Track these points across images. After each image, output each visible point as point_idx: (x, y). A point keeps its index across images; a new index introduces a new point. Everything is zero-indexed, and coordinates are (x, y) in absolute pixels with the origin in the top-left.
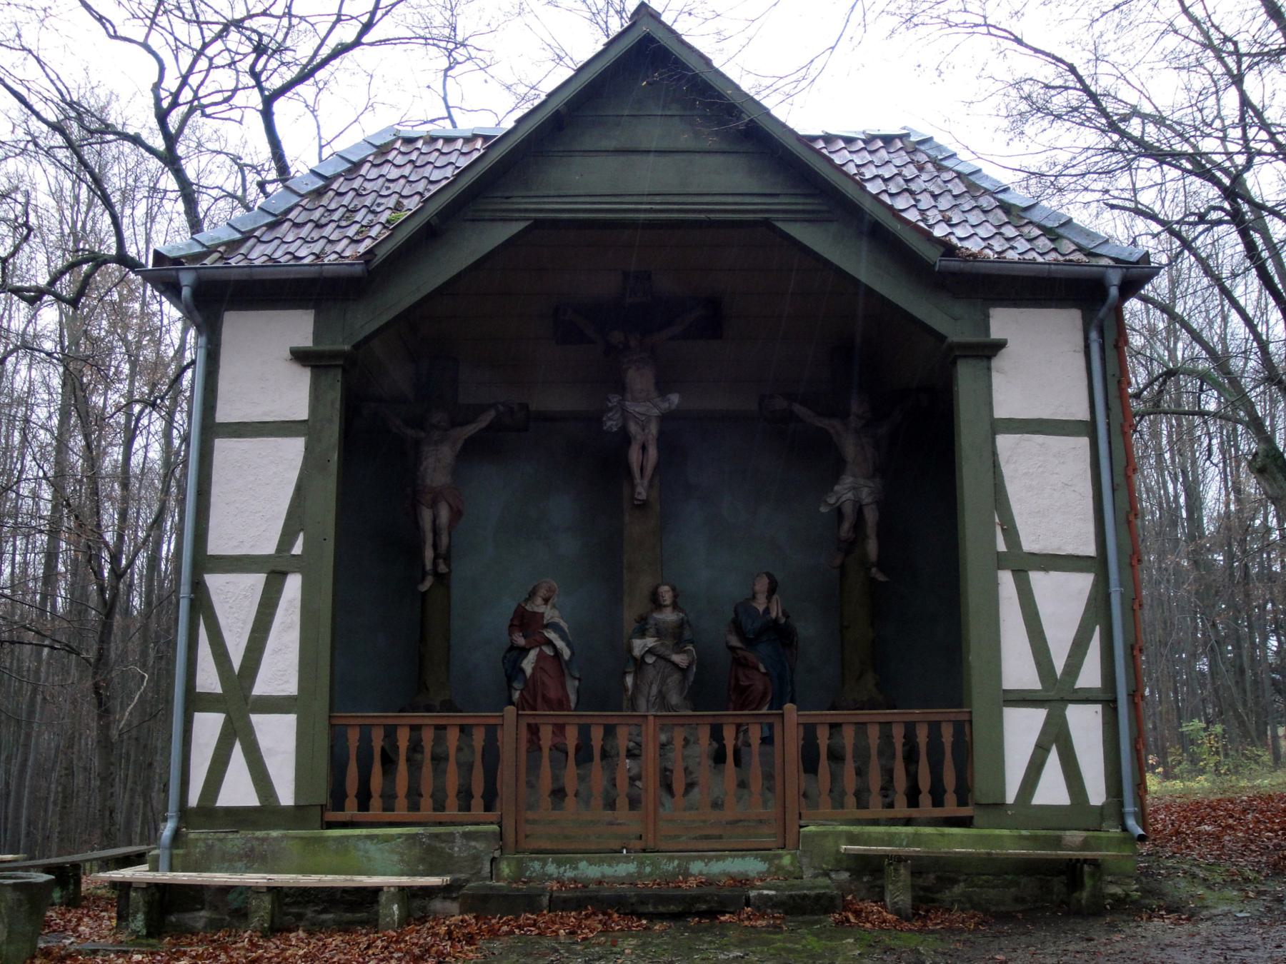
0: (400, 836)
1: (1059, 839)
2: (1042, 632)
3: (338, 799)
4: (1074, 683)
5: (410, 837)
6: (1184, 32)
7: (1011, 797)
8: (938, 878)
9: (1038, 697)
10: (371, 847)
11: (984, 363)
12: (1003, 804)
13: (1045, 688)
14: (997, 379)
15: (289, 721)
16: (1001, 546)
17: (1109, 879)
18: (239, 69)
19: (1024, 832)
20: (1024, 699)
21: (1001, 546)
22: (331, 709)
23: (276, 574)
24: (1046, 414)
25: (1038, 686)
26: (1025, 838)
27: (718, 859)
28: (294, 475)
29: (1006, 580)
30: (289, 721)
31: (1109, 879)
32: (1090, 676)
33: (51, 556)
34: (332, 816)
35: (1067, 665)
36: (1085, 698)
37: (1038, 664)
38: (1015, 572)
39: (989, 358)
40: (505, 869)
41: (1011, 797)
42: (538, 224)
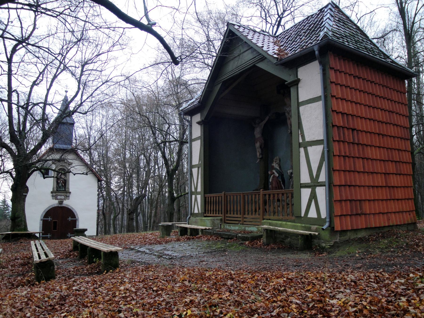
0: (209, 219)
1: (310, 228)
2: (311, 165)
3: (205, 210)
4: (318, 180)
5: (211, 219)
6: (27, 32)
7: (303, 215)
8: (285, 236)
9: (309, 185)
10: (207, 221)
11: (296, 86)
12: (301, 217)
13: (311, 183)
14: (300, 90)
15: (302, 181)
16: (301, 141)
17: (322, 241)
18: (126, 81)
19: (303, 225)
20: (306, 186)
21: (301, 141)
22: (204, 194)
23: (199, 168)
24: (311, 97)
25: (310, 182)
26: (303, 227)
27: (249, 227)
28: (199, 147)
29: (302, 150)
30: (302, 181)
31: (322, 241)
32: (323, 178)
33: (416, 129)
34: (207, 214)
35: (316, 175)
36: (321, 185)
37: (310, 175)
38: (304, 148)
39: (297, 84)
40: (222, 227)
41: (303, 215)
42: (223, 82)
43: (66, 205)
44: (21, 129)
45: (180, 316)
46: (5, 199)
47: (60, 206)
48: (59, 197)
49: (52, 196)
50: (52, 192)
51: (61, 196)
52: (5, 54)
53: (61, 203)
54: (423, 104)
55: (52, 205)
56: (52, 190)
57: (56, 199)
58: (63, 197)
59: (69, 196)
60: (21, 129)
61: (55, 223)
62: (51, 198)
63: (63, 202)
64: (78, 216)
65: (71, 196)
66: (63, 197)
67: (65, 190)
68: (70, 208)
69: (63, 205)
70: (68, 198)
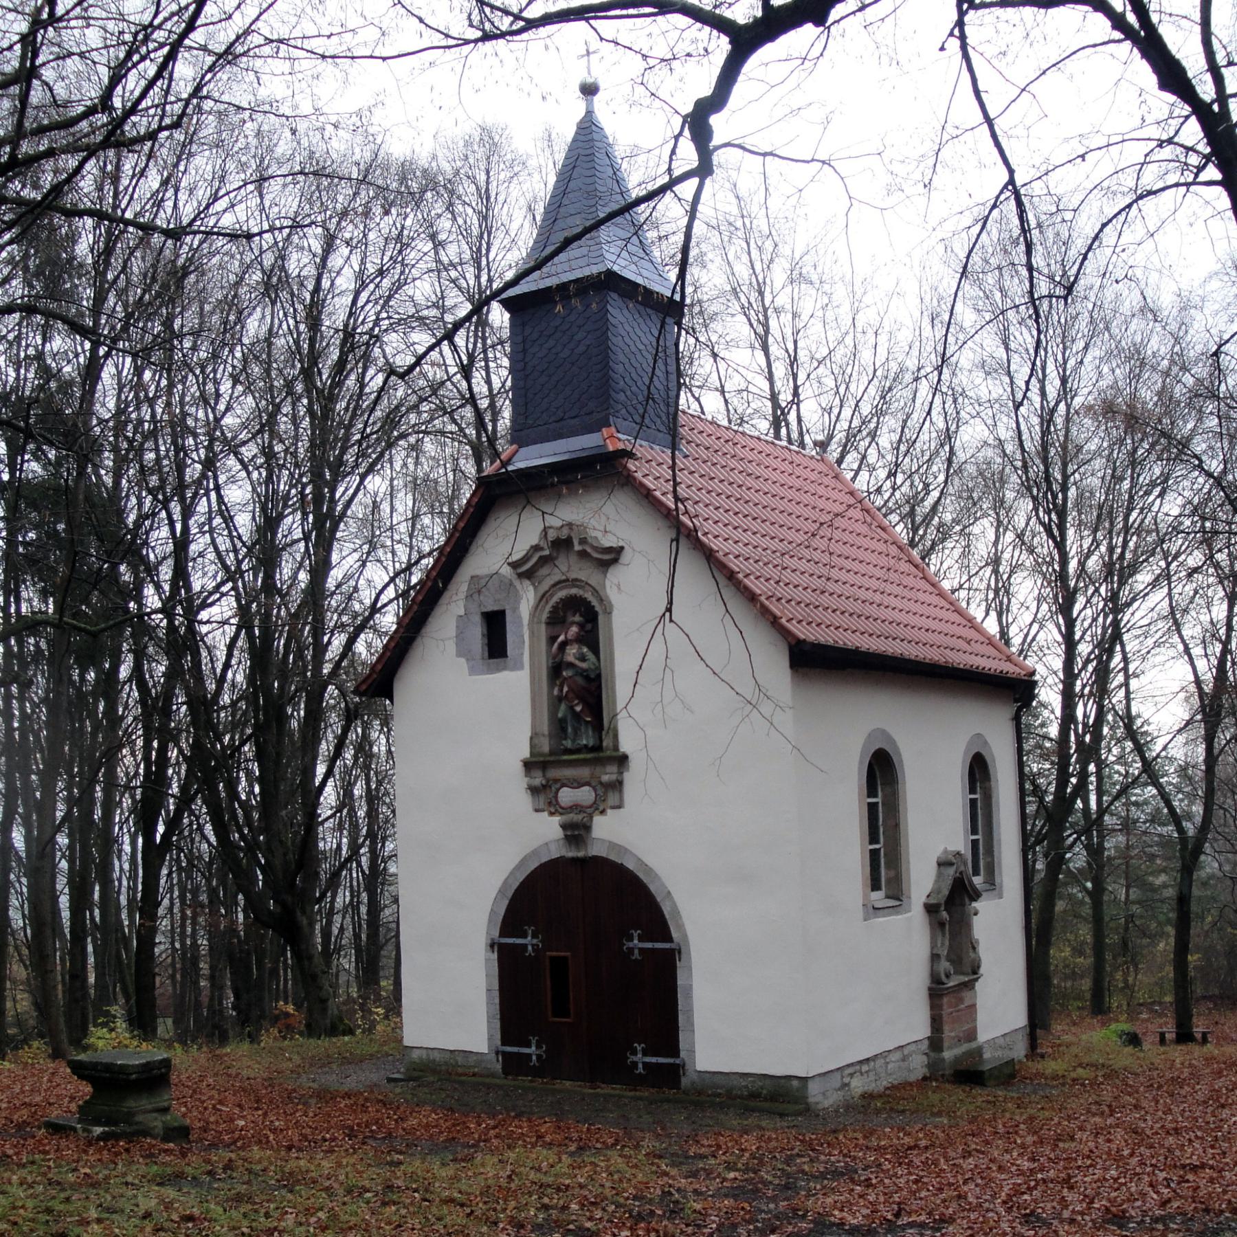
43: (613, 846)
44: (97, 919)
45: (1233, 925)
46: (588, 130)
47: (571, 854)
48: (567, 796)
49: (534, 790)
50: (528, 765)
51: (577, 784)
52: (747, 154)
53: (576, 832)
54: (4, 796)
55: (535, 853)
56: (526, 753)
57: (553, 807)
58: (585, 795)
59: (618, 785)
60: (97, 919)
61: (559, 966)
62: (524, 801)
63: (587, 828)
64: (681, 927)
65: (633, 779)
66: (585, 795)
67: (598, 748)
68: (630, 865)
69: (595, 850)
70: (612, 799)
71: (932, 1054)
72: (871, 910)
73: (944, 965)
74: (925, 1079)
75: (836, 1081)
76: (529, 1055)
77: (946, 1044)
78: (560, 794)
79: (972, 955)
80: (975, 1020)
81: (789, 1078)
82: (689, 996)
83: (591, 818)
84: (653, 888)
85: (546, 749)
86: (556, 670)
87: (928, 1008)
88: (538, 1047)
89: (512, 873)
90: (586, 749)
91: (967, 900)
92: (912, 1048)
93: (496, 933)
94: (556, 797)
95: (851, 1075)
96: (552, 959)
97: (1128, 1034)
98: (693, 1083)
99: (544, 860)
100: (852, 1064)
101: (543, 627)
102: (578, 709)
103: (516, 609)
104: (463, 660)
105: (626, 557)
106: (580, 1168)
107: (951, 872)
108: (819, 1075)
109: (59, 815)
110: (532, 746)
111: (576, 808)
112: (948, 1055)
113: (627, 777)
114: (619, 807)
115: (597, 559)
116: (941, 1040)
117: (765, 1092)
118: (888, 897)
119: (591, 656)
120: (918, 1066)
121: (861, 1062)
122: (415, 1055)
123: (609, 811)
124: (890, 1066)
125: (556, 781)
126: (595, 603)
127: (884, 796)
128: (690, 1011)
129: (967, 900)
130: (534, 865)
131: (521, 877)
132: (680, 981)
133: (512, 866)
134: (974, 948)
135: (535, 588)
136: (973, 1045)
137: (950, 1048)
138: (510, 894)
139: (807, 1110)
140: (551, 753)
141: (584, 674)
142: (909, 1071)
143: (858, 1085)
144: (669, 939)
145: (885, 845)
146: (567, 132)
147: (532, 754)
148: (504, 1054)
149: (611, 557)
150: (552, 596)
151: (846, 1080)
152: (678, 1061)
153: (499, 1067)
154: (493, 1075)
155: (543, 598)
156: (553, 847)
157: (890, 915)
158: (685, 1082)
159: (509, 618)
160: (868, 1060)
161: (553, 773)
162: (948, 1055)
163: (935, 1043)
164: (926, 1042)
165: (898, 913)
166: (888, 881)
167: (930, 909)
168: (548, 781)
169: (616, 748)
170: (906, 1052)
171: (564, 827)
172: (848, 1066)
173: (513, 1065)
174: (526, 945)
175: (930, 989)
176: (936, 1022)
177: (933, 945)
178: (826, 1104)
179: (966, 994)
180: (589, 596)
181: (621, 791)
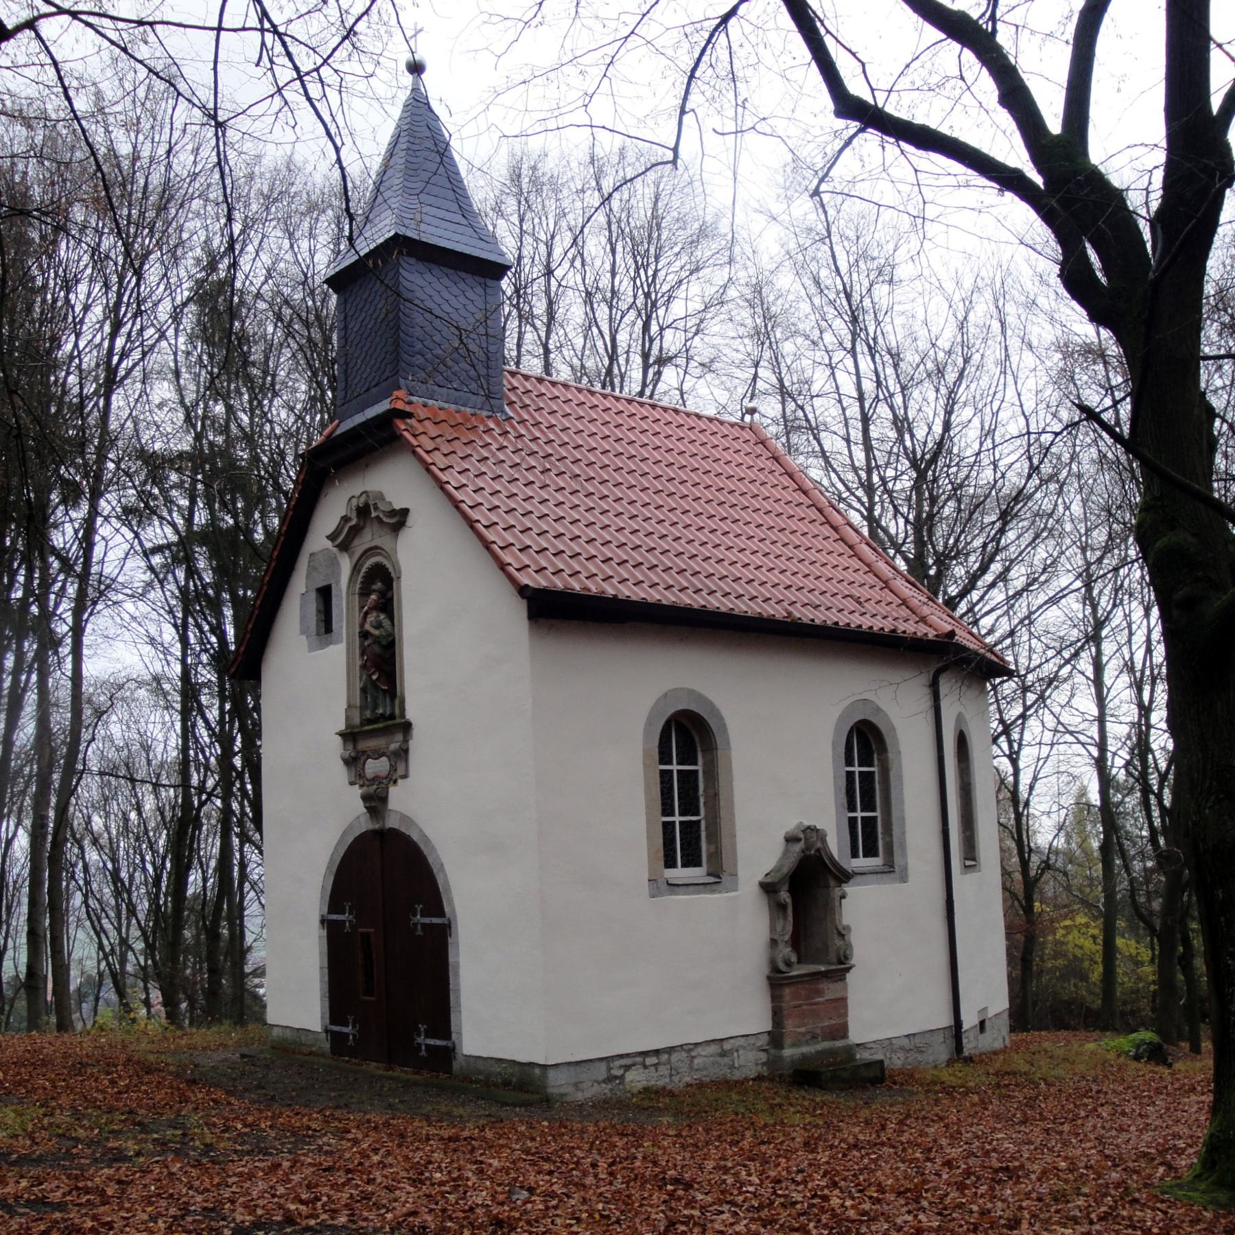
43: (404, 818)
55: (351, 827)
63: (384, 800)
65: (418, 745)
68: (415, 837)
69: (392, 823)
71: (772, 1051)
72: (665, 886)
73: (786, 951)
74: (759, 1078)
75: (601, 1072)
76: (347, 1035)
77: (788, 1041)
78: (367, 767)
79: (838, 942)
80: (846, 1015)
81: (532, 1065)
82: (457, 975)
83: (387, 788)
84: (430, 860)
85: (357, 721)
86: (364, 635)
87: (769, 1000)
88: (354, 1027)
89: (336, 848)
90: (383, 717)
91: (832, 883)
92: (742, 1041)
93: (326, 910)
94: (363, 769)
95: (627, 1068)
96: (362, 934)
97: (1149, 1044)
98: (461, 1068)
99: (357, 834)
100: (627, 1055)
101: (357, 597)
102: (374, 677)
103: (338, 582)
104: (304, 637)
105: (411, 520)
106: (611, 1165)
107: (798, 847)
108: (569, 1064)
109: (196, 803)
110: (348, 718)
111: (376, 779)
112: (788, 1052)
113: (412, 744)
114: (405, 776)
115: (388, 524)
116: (781, 1035)
117: (514, 1080)
118: (709, 874)
119: (386, 623)
120: (749, 1063)
121: (645, 1054)
122: (276, 1032)
123: (400, 781)
124: (696, 1061)
125: (364, 752)
126: (391, 570)
127: (705, 764)
128: (458, 991)
129: (832, 883)
130: (350, 839)
131: (342, 852)
132: (451, 960)
133: (335, 842)
134: (842, 936)
135: (350, 557)
136: (839, 1044)
137: (794, 1045)
138: (334, 869)
139: (546, 1101)
140: (362, 724)
141: (377, 640)
142: (732, 1067)
143: (637, 1079)
144: (442, 914)
145: (706, 818)
146: (404, 96)
147: (347, 727)
148: (333, 1033)
149: (399, 519)
150: (362, 566)
151: (616, 1072)
152: (450, 1044)
153: (327, 1046)
154: (323, 1055)
155: (356, 569)
156: (363, 819)
157: (699, 893)
158: (456, 1066)
159: (334, 592)
160: (657, 1052)
161: (365, 745)
162: (788, 1052)
163: (776, 1038)
164: (766, 1038)
165: (713, 892)
166: (710, 857)
167: (768, 888)
168: (358, 752)
169: (403, 714)
170: (727, 1046)
171: (365, 798)
172: (621, 1056)
173: (337, 1040)
174: (344, 922)
175: (769, 978)
176: (777, 1015)
177: (773, 928)
178: (580, 1096)
179: (830, 990)
180: (388, 565)
181: (407, 761)
